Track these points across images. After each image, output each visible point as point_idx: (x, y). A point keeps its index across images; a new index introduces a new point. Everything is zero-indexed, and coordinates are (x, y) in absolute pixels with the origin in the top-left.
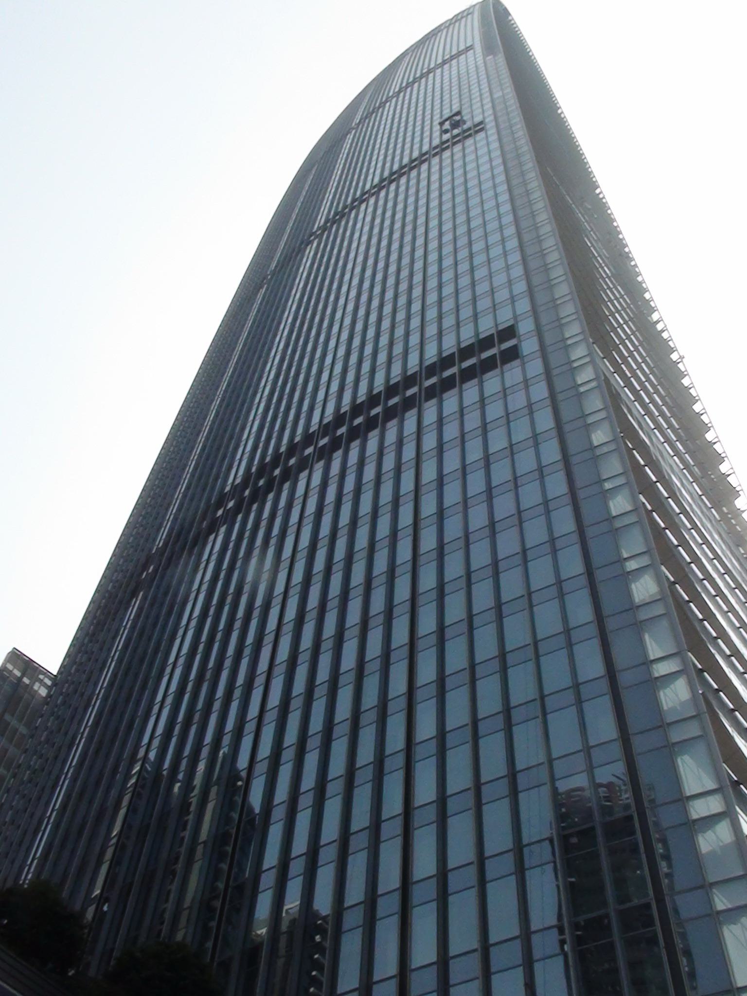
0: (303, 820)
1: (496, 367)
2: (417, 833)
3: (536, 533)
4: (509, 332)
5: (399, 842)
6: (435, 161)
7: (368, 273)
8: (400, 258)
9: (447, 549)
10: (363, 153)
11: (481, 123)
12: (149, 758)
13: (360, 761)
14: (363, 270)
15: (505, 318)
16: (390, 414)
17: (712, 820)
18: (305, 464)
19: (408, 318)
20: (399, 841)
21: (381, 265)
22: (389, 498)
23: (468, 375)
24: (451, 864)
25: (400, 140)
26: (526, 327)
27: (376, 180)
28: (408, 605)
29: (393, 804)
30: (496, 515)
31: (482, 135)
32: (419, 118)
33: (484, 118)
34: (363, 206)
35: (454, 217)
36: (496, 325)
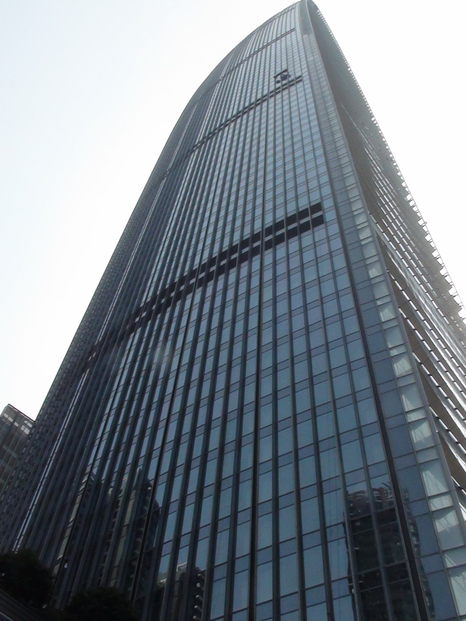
0: (189, 511)
1: (310, 229)
2: (260, 519)
3: (334, 332)
4: (318, 207)
5: (249, 525)
6: (272, 100)
7: (230, 170)
8: (249, 161)
9: (279, 342)
10: (226, 96)
11: (300, 77)
12: (93, 473)
13: (225, 475)
14: (227, 168)
15: (315, 198)
16: (243, 258)
17: (444, 511)
19: (255, 198)
20: (249, 524)
21: (238, 165)
22: (243, 310)
23: (292, 234)
24: (282, 539)
25: (250, 87)
26: (328, 204)
27: (235, 112)
28: (254, 377)
29: (245, 501)
30: (309, 321)
31: (300, 84)
32: (261, 74)
33: (302, 74)
34: (227, 129)
35: (283, 135)
36: (310, 203)
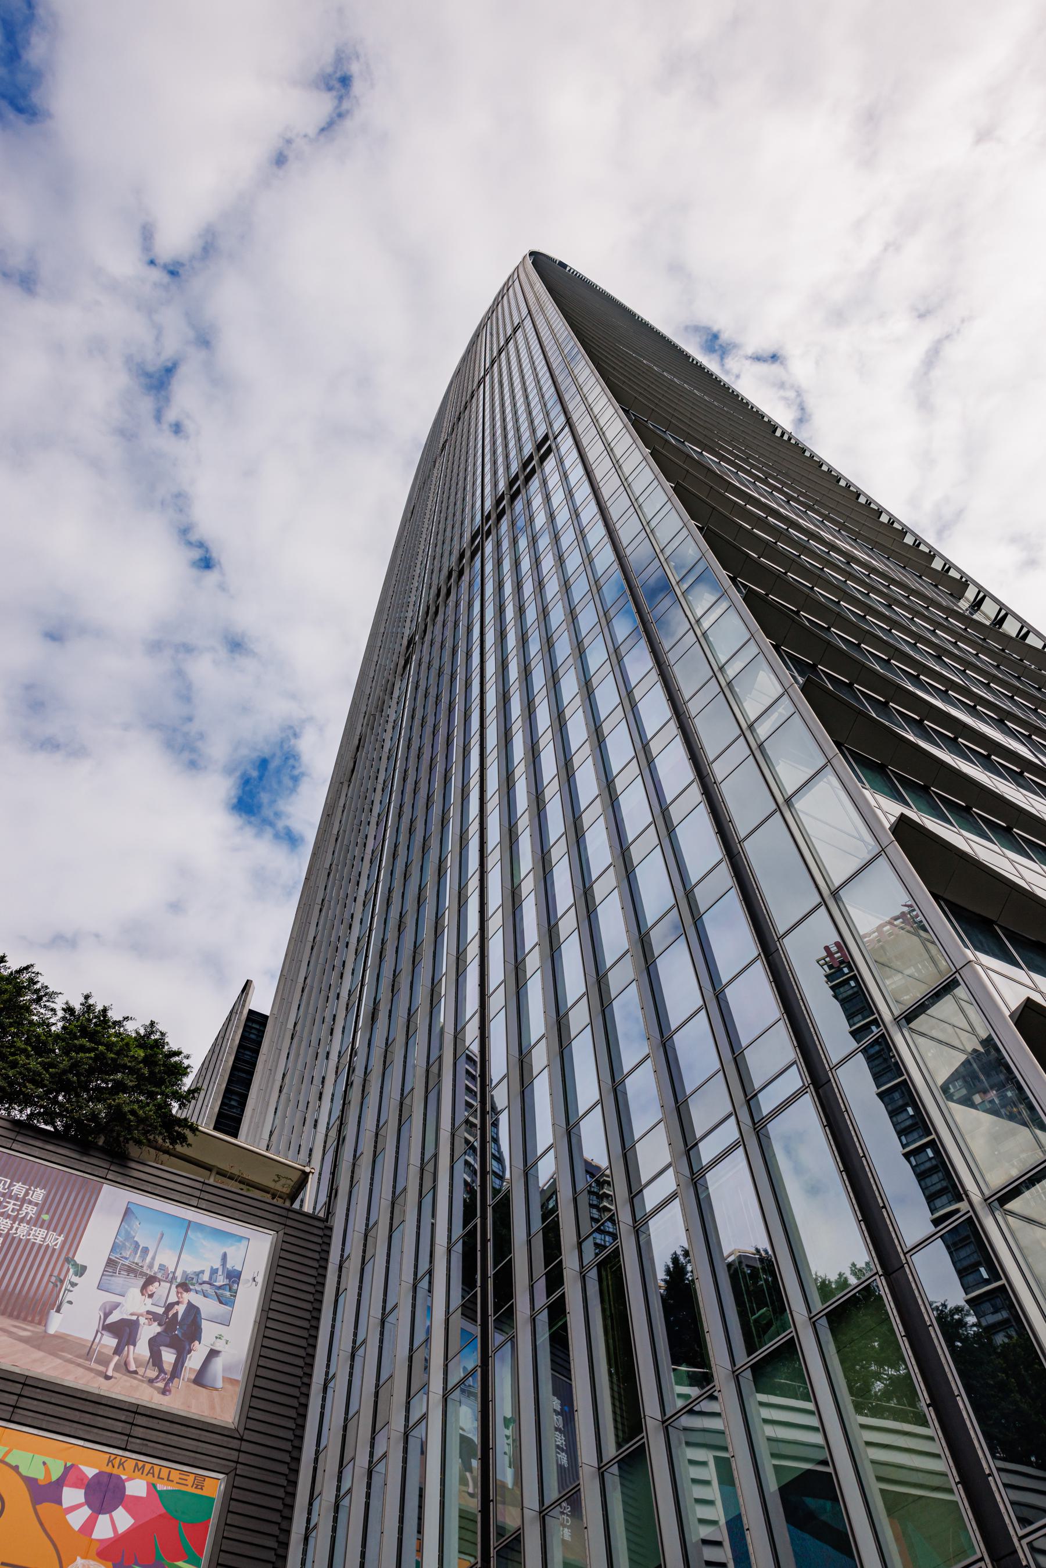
11: (546, 438)
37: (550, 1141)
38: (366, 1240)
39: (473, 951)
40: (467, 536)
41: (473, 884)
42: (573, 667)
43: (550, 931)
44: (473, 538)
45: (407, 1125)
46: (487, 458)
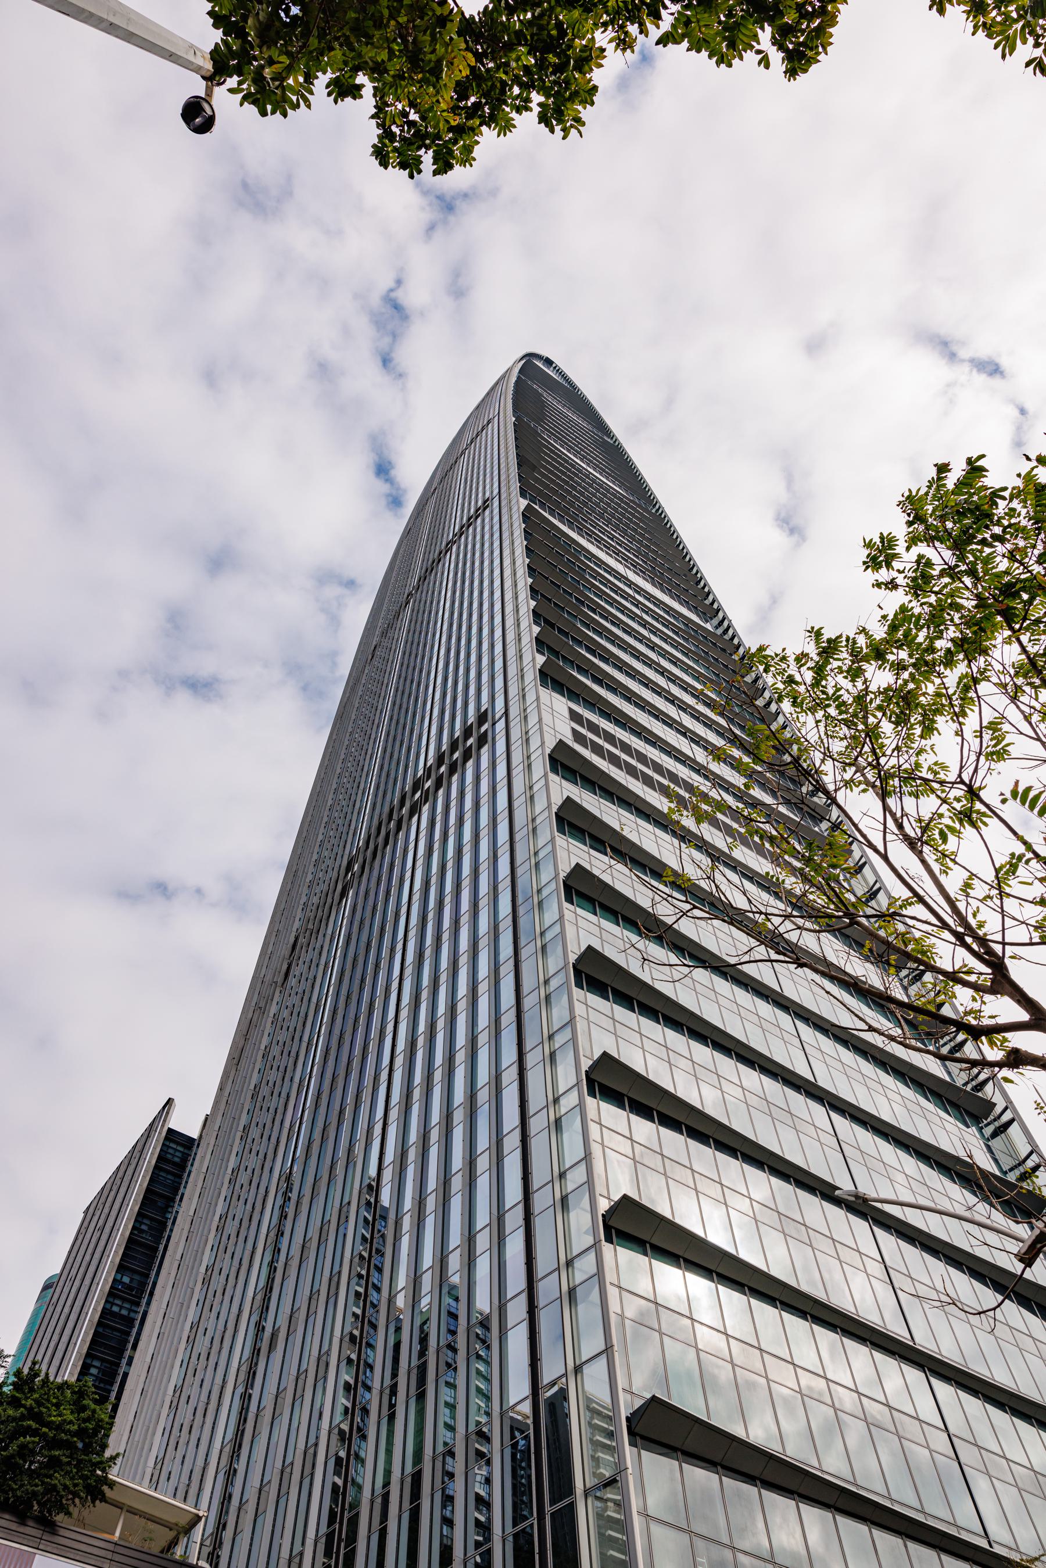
11: (488, 499)
18: (415, 809)
37: (410, 1207)
38: (260, 1493)
39: (395, 985)
40: (444, 544)
41: (399, 947)
42: (460, 1193)
43: (428, 1077)
44: (447, 545)
45: (333, 1181)
46: (460, 502)
